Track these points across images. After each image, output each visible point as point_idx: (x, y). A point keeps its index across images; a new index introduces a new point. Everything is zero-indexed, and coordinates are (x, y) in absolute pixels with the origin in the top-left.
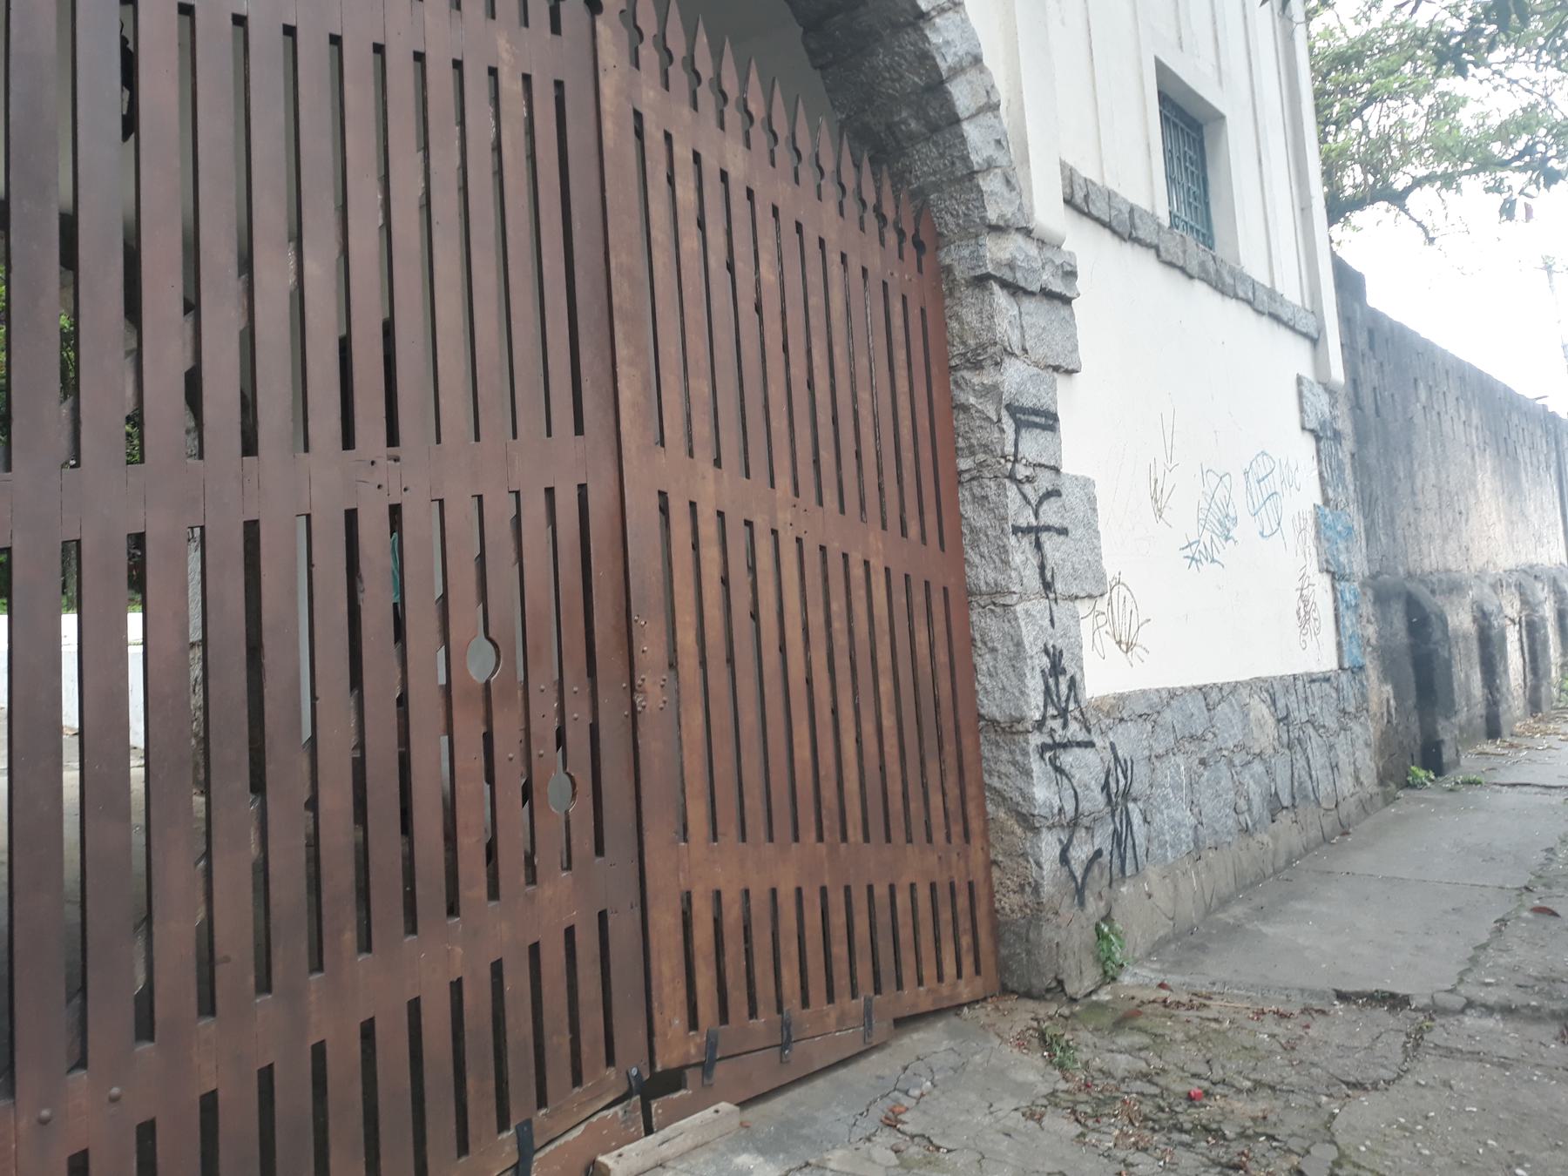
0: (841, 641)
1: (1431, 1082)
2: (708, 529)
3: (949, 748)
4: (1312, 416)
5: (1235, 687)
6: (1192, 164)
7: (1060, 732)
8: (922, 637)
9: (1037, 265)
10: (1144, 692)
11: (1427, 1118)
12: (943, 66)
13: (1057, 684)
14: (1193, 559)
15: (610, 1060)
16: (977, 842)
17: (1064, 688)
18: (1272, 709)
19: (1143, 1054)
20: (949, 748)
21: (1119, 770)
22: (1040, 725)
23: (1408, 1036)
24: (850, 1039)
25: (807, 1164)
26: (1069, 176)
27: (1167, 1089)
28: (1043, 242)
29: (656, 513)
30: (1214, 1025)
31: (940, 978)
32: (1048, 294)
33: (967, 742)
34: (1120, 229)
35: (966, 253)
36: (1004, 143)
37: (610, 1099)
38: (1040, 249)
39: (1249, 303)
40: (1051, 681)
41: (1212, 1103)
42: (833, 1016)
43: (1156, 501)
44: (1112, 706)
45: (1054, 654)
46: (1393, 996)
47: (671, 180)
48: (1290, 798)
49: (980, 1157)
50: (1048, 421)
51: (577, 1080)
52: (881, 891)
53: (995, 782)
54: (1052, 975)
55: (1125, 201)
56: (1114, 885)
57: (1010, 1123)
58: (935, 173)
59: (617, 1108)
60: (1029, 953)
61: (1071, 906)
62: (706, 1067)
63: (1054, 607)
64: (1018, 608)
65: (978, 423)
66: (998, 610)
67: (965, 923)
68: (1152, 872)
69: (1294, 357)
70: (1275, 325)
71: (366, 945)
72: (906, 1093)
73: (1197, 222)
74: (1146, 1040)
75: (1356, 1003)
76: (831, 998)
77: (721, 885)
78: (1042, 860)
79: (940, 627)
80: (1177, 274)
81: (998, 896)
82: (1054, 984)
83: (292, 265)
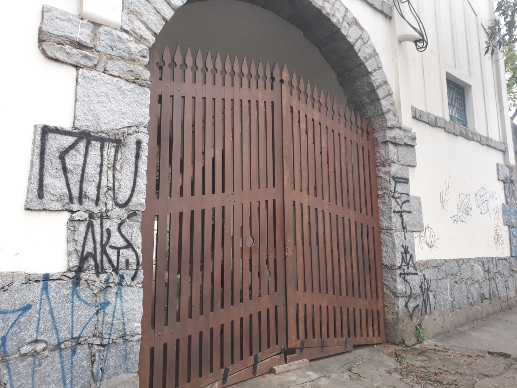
0: (341, 241)
1: (509, 377)
2: (305, 210)
3: (373, 272)
4: (502, 176)
5: (469, 260)
6: (460, 100)
7: (407, 270)
8: (365, 241)
9: (403, 137)
10: (436, 260)
11: (504, 385)
12: (375, 85)
13: (406, 256)
14: (455, 220)
15: (277, 344)
16: (380, 299)
17: (408, 257)
18: (483, 268)
19: (425, 362)
20: (373, 272)
21: (426, 282)
22: (400, 267)
23: (507, 365)
24: (341, 348)
25: (326, 376)
26: (414, 110)
27: (430, 371)
28: (405, 130)
29: (292, 206)
30: (448, 357)
31: (368, 336)
32: (406, 145)
33: (378, 271)
34: (432, 124)
35: (381, 135)
36: (394, 104)
37: (276, 353)
38: (404, 132)
39: (478, 142)
40: (404, 255)
41: (442, 376)
42: (336, 341)
43: (442, 203)
44: (424, 264)
45: (405, 248)
46: (506, 354)
47: (299, 122)
48: (489, 296)
49: (371, 380)
50: (406, 181)
51: (269, 347)
52: (351, 310)
53: (387, 283)
54: (401, 339)
55: (433, 115)
56: (423, 315)
57: (382, 374)
58: (373, 113)
59: (278, 356)
60: (395, 332)
61: (408, 320)
62: (301, 349)
63: (406, 234)
64: (394, 234)
65: (384, 181)
66: (388, 234)
67: (376, 321)
68: (436, 313)
69: (497, 157)
70: (488, 148)
71: (222, 306)
72: (355, 363)
73: (461, 118)
74: (427, 358)
75: (494, 355)
76: (335, 337)
77: (306, 303)
78: (399, 306)
79: (371, 238)
80: (452, 135)
81: (386, 315)
82: (402, 341)
83: (213, 152)
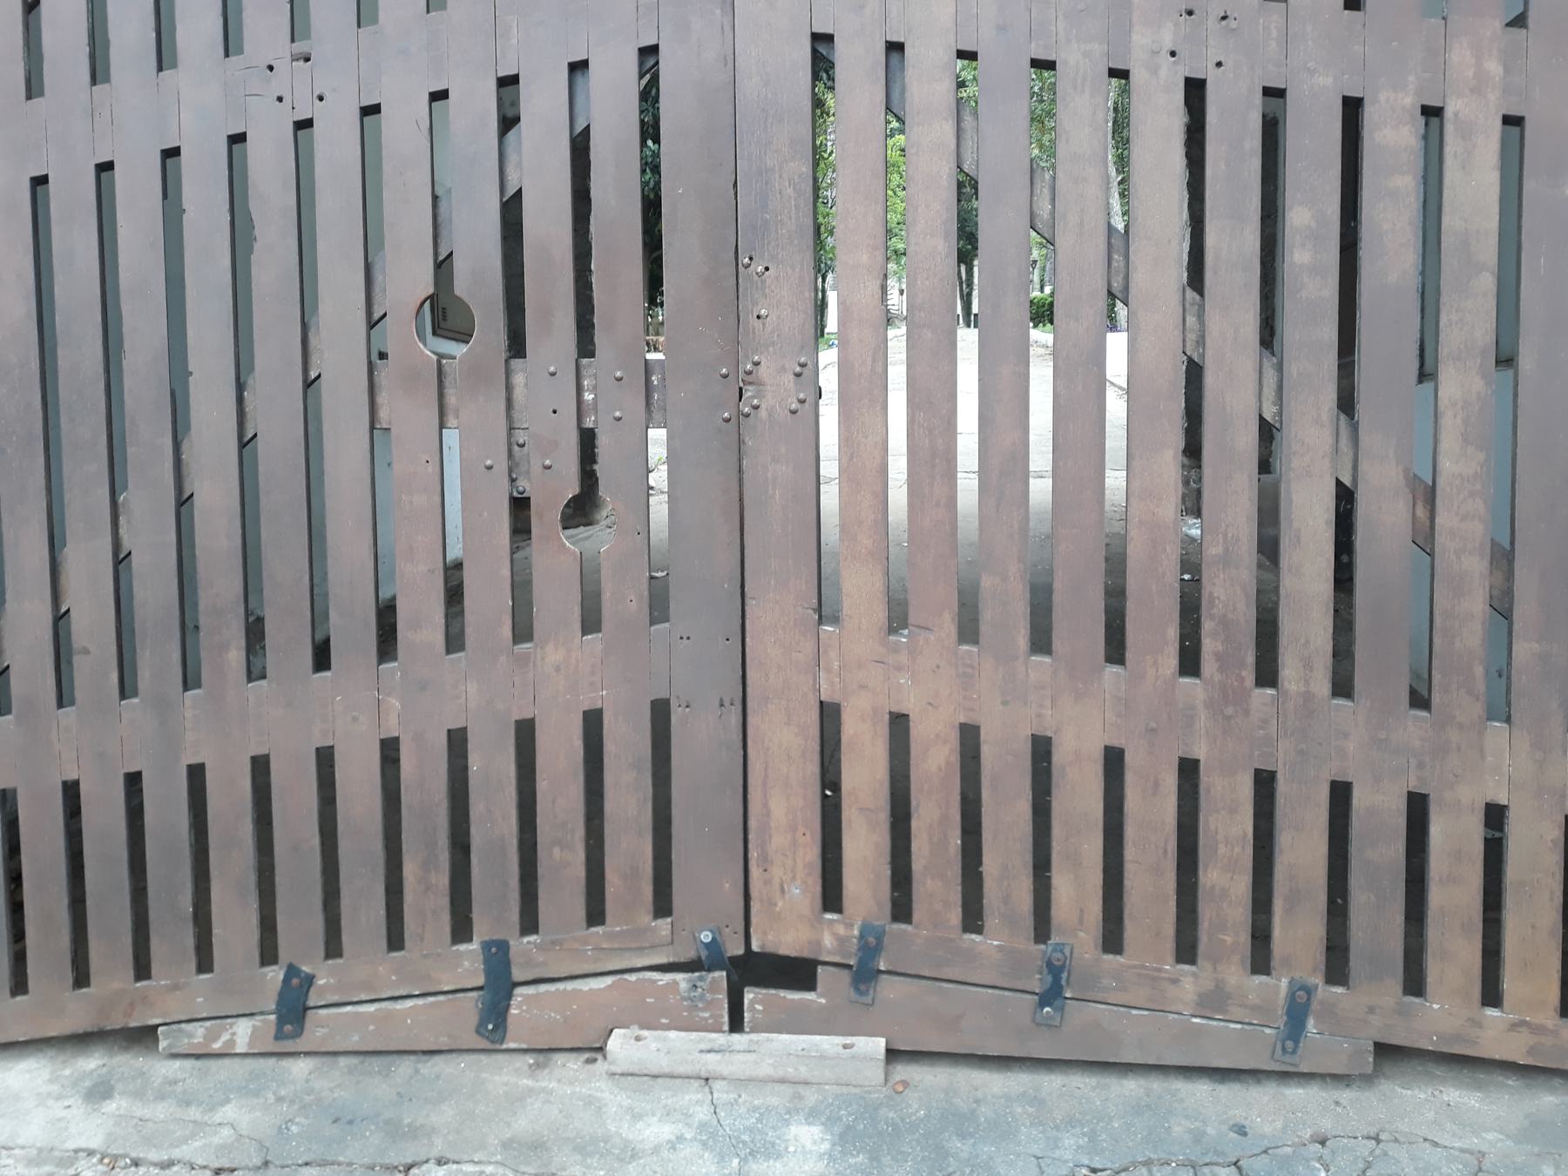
15: (663, 906)
59: (681, 978)
62: (864, 974)
77: (909, 704)
